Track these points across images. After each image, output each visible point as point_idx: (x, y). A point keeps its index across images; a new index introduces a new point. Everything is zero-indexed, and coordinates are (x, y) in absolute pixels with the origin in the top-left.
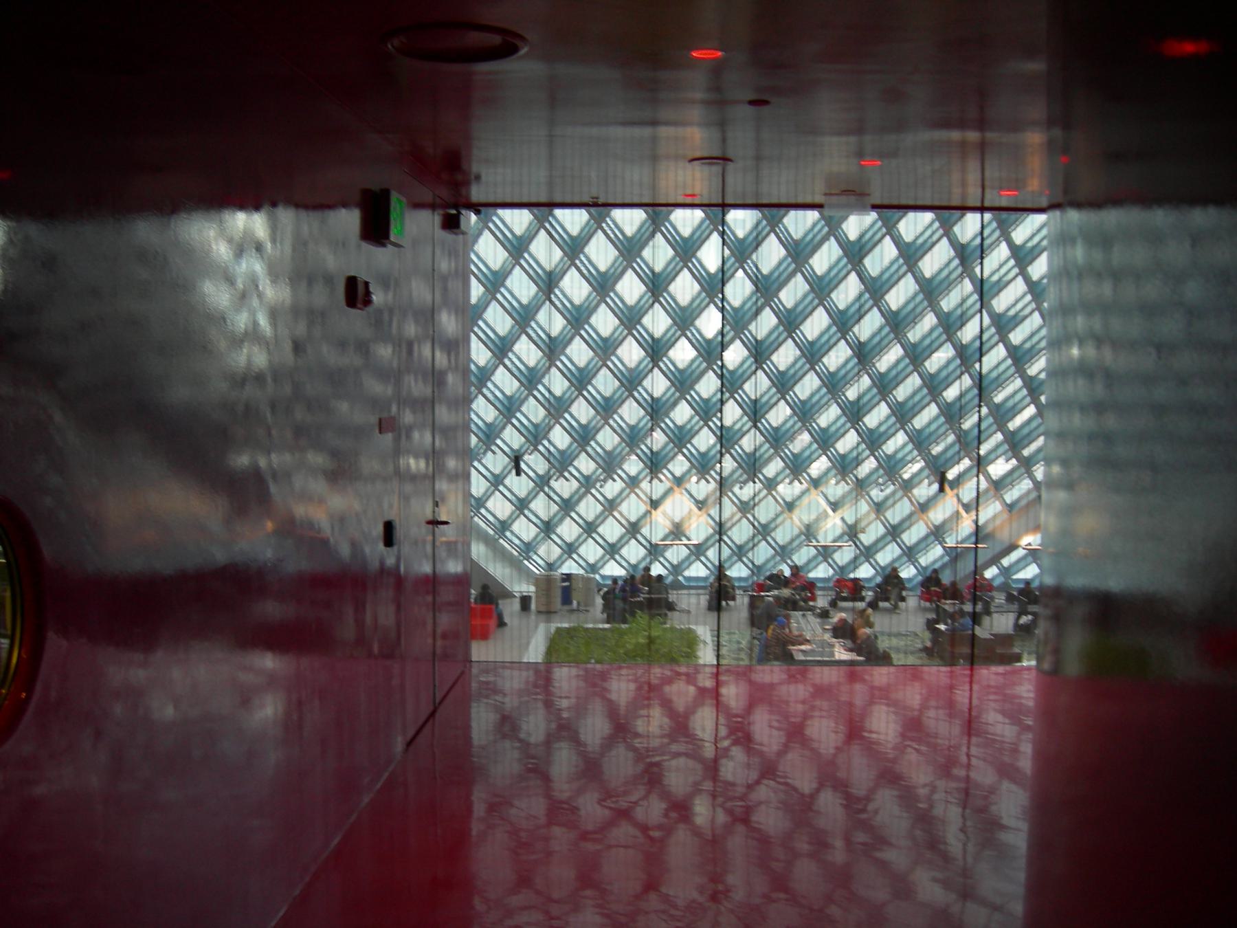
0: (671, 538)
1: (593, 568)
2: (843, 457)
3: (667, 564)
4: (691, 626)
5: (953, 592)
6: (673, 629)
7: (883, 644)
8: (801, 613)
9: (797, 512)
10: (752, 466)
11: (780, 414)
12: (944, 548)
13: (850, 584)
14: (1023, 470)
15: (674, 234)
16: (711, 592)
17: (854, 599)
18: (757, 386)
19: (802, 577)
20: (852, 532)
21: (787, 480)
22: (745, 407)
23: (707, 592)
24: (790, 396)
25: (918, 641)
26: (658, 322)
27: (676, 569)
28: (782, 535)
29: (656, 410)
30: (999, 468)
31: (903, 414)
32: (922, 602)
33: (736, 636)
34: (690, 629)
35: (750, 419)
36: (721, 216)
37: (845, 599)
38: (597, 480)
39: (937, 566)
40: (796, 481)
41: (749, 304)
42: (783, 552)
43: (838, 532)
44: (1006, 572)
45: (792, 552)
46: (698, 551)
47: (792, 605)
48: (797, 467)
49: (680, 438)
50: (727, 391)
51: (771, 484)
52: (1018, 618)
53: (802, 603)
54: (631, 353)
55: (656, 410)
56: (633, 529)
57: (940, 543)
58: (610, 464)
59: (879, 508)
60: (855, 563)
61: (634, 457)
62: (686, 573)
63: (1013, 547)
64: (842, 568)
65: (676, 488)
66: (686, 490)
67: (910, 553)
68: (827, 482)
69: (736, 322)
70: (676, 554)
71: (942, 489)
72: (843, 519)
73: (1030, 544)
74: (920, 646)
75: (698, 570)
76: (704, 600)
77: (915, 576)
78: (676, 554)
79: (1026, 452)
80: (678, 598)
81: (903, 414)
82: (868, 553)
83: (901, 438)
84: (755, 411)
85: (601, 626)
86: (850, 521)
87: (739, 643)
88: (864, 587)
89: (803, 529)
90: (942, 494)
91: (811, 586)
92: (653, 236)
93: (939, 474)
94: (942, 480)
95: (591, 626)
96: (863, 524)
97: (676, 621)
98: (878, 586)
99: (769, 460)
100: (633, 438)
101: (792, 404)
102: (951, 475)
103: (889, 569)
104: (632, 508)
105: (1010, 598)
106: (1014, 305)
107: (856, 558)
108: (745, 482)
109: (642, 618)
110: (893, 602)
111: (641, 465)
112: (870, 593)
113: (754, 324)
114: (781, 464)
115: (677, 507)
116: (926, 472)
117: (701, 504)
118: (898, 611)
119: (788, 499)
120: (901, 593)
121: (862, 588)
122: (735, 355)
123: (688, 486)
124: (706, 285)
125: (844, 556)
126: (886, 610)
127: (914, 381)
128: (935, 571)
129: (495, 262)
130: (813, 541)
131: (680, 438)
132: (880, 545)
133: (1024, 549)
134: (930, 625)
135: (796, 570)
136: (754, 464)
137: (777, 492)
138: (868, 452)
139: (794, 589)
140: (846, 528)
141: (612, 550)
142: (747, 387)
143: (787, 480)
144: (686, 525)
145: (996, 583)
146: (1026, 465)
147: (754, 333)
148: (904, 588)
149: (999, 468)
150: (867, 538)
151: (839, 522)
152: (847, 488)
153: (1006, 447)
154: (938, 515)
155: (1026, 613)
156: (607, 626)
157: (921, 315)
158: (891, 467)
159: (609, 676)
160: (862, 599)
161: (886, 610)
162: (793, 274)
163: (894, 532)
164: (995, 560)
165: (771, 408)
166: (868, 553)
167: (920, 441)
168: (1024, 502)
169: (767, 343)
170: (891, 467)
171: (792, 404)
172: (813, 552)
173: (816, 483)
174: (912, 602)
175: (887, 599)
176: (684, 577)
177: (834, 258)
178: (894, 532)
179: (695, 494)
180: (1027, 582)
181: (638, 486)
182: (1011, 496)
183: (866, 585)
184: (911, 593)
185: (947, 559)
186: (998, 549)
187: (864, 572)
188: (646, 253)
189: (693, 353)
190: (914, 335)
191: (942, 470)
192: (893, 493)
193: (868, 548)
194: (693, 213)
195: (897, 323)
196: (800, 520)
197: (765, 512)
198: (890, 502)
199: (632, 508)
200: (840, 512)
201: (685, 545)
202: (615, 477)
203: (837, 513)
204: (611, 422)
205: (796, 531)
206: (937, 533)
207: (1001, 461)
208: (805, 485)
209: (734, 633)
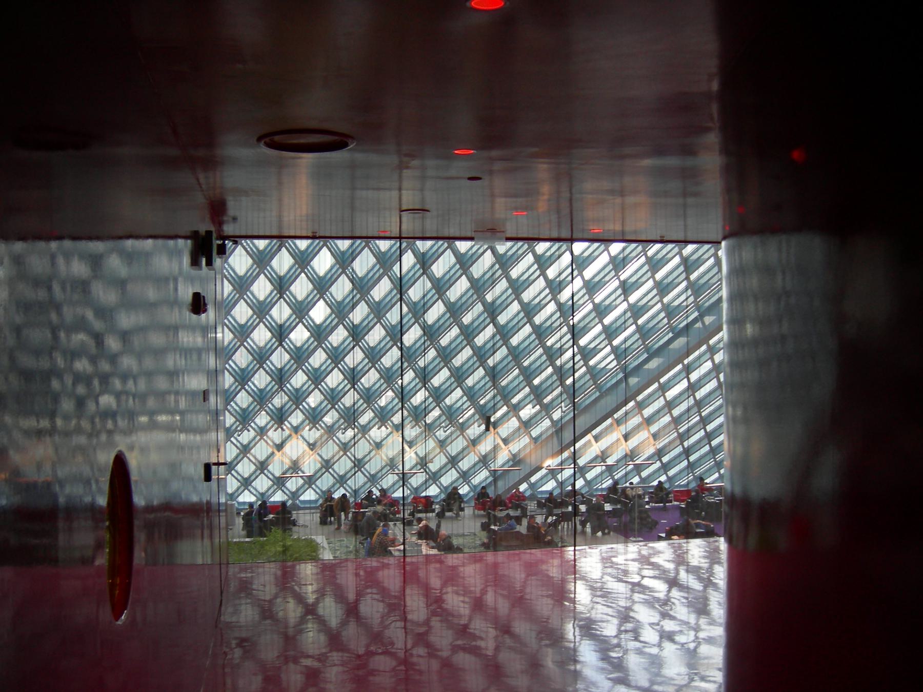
0: (291, 471)
1: (232, 496)
2: (416, 408)
3: (318, 490)
4: (312, 537)
5: (498, 503)
6: (299, 539)
7: (455, 542)
8: (393, 523)
9: (384, 449)
10: (350, 417)
11: (371, 378)
12: (489, 471)
13: (423, 500)
14: (544, 413)
15: (294, 248)
16: (321, 510)
17: (426, 512)
18: (355, 358)
19: (389, 497)
20: (423, 462)
21: (377, 426)
22: (346, 373)
23: (319, 511)
24: (342, 365)
25: (477, 539)
26: (281, 312)
27: (295, 495)
28: (373, 467)
29: (281, 377)
30: (527, 412)
31: (459, 376)
32: (476, 511)
33: (344, 542)
34: (312, 541)
35: (349, 382)
36: (183, 234)
37: (420, 511)
38: (236, 431)
39: (484, 484)
40: (383, 427)
41: (348, 300)
42: (373, 479)
43: (414, 462)
44: (532, 486)
45: (382, 478)
46: (310, 481)
47: (384, 517)
48: (383, 417)
49: (298, 397)
50: (406, 361)
51: (365, 430)
52: (546, 519)
53: (391, 516)
54: (261, 336)
55: (281, 377)
56: (262, 466)
57: (486, 468)
58: (245, 418)
59: (442, 444)
60: (425, 485)
61: (263, 412)
62: (302, 498)
63: (539, 468)
64: (416, 489)
65: (294, 435)
66: (301, 435)
67: (465, 476)
68: (304, 428)
69: (340, 311)
70: (292, 484)
71: (487, 429)
72: (416, 453)
73: (549, 466)
74: (478, 542)
75: (309, 495)
76: (317, 517)
77: (469, 492)
78: (292, 484)
79: (514, 401)
80: (297, 517)
81: (459, 376)
82: (434, 477)
83: (458, 392)
84: (353, 376)
85: (242, 540)
86: (422, 454)
87: (347, 547)
88: (433, 502)
89: (389, 462)
90: (488, 432)
91: (394, 502)
92: (280, 250)
93: (485, 418)
94: (488, 423)
95: (238, 540)
96: (431, 456)
97: (298, 533)
98: (444, 500)
99: (363, 412)
100: (262, 398)
101: (307, 371)
102: (492, 420)
103: (451, 488)
104: (261, 451)
105: (540, 505)
106: (535, 297)
107: (426, 481)
108: (346, 429)
109: (277, 533)
110: (455, 512)
111: (269, 418)
112: (437, 506)
113: (351, 314)
114: (372, 414)
115: (295, 448)
116: (477, 417)
117: (312, 446)
118: (459, 519)
119: (378, 440)
120: (460, 505)
121: (432, 503)
122: (339, 336)
123: (302, 433)
124: (317, 285)
125: (417, 480)
126: (451, 518)
127: (467, 352)
128: (483, 488)
129: (241, 271)
130: (299, 472)
131: (298, 397)
132: (443, 471)
133: (546, 469)
134: (485, 527)
135: (383, 491)
136: (282, 417)
137: (267, 437)
138: (434, 404)
139: (385, 505)
140: (418, 460)
141: (246, 483)
142: (347, 359)
143: (377, 426)
144: (301, 462)
145: (527, 494)
146: (547, 409)
147: (390, 319)
148: (462, 501)
149: (527, 412)
150: (433, 467)
151: (413, 455)
152: (318, 434)
153: (532, 397)
154: (485, 447)
155: (552, 515)
156: (247, 540)
157: (473, 305)
158: (451, 414)
159: (319, 576)
160: (433, 511)
161: (451, 518)
162: (258, 275)
163: (453, 461)
164: (526, 478)
165: (327, 375)
166: (434, 477)
167: (471, 395)
168: (544, 437)
169: (361, 328)
170: (451, 414)
171: (307, 371)
172: (301, 481)
173: (296, 429)
174: (468, 511)
175: (450, 510)
176: (300, 501)
177: (370, 264)
178: (453, 461)
179: (307, 438)
180: (551, 493)
181: (266, 434)
182: (535, 433)
183: (435, 501)
184: (466, 505)
185: (491, 479)
186: (528, 471)
187: (433, 491)
188: (274, 263)
189: (269, 335)
190: (467, 319)
191: (488, 415)
192: (452, 433)
193: (435, 474)
194: (295, 233)
195: (454, 311)
196: (387, 456)
197: (362, 448)
198: (449, 440)
199: (261, 451)
200: (414, 448)
201: (301, 476)
202: (249, 428)
203: (413, 449)
204: (246, 387)
205: (384, 464)
206: (484, 460)
207: (530, 406)
208: (390, 429)
209: (343, 541)
